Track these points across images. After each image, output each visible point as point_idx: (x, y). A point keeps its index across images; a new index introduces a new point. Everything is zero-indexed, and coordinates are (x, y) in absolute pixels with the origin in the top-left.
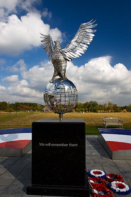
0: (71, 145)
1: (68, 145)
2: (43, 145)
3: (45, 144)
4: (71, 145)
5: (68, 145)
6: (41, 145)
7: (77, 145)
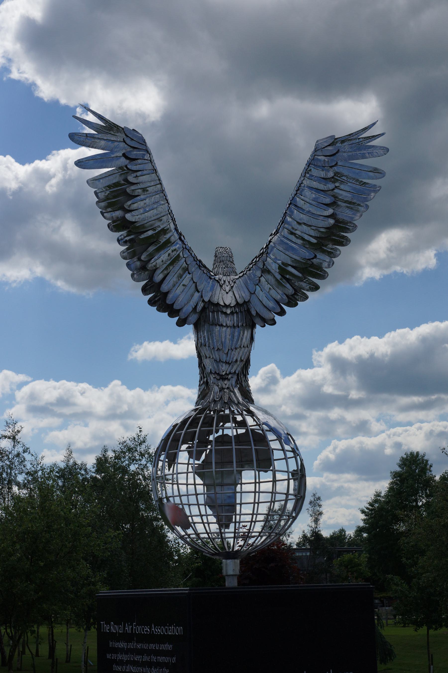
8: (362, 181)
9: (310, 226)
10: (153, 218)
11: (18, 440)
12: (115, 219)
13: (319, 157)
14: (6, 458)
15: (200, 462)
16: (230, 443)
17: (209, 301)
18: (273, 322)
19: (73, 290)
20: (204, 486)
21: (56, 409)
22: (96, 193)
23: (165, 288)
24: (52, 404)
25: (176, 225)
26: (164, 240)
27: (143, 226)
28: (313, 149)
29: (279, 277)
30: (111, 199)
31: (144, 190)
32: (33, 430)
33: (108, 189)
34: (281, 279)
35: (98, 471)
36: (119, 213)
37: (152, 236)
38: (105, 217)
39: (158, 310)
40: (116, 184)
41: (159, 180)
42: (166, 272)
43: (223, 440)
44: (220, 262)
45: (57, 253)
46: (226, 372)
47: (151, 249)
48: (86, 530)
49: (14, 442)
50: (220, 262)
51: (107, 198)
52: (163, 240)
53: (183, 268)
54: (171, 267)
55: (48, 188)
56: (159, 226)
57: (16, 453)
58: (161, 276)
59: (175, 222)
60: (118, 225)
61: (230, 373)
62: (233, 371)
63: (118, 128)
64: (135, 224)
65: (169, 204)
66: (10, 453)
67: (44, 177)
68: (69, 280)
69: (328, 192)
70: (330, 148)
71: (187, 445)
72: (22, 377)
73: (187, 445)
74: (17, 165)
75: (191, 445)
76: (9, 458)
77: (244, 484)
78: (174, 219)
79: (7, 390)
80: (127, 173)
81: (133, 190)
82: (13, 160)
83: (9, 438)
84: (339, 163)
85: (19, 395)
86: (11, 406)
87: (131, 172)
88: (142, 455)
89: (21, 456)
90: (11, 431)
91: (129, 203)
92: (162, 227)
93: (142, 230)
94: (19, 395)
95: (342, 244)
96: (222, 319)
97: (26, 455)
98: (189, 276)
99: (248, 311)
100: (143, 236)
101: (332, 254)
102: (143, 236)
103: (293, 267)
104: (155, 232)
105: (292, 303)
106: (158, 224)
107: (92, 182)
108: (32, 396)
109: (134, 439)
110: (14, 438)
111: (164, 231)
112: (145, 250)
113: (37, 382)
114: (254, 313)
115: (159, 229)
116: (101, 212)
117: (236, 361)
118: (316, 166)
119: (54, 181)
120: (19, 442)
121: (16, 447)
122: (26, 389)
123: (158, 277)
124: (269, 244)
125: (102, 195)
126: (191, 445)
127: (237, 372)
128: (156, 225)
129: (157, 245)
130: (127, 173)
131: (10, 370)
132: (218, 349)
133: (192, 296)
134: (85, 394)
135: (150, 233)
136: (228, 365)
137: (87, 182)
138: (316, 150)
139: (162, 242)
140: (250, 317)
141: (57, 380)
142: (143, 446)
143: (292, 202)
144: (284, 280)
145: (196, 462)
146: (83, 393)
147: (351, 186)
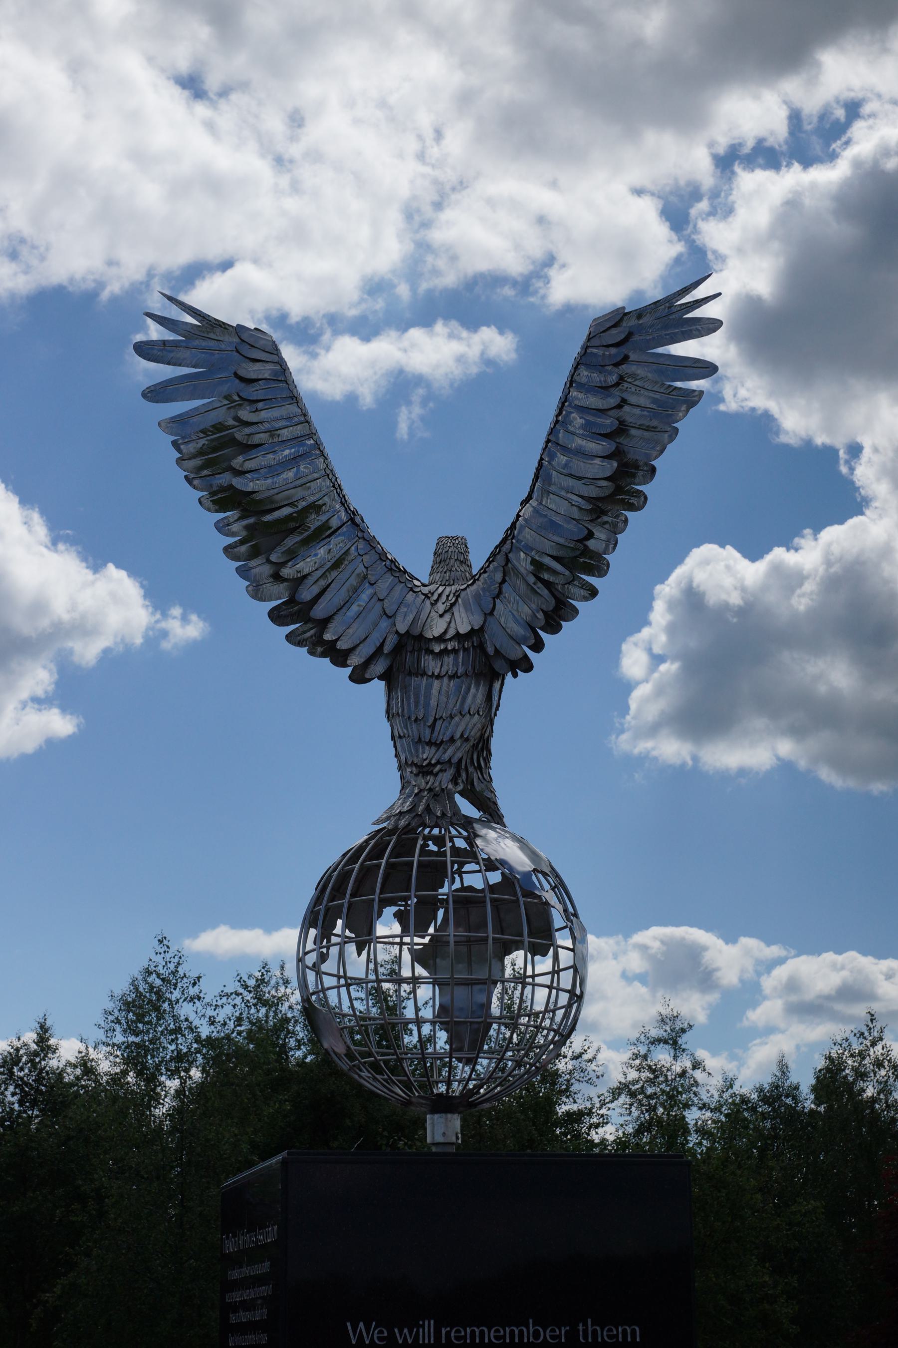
0: (587, 1330)
1: (572, 1335)
2: (375, 1334)
3: (392, 1334)
4: (594, 1333)
5: (572, 1335)
6: (405, 1339)
7: (633, 1332)
8: (670, 386)
9: (580, 478)
10: (292, 485)
11: (683, 1047)
12: (215, 488)
13: (595, 351)
14: (661, 1079)
15: (427, 940)
16: (481, 902)
17: (408, 632)
18: (528, 667)
19: (851, 783)
20: (434, 987)
21: (839, 1007)
22: (175, 444)
23: (319, 611)
24: (828, 998)
25: (344, 497)
26: (318, 524)
27: (270, 499)
28: (584, 337)
29: (531, 579)
30: (209, 454)
31: (272, 432)
32: (798, 1047)
33: (202, 435)
34: (534, 584)
35: (818, 1101)
36: (225, 479)
37: (289, 518)
38: (194, 487)
39: (311, 653)
40: (219, 427)
41: (305, 415)
42: (323, 583)
43: (467, 900)
44: (440, 562)
45: (812, 715)
46: (431, 760)
47: (291, 541)
48: (752, 1198)
49: (675, 1050)
50: (440, 562)
51: (200, 453)
52: (314, 522)
53: (359, 575)
54: (334, 574)
55: (794, 601)
56: (303, 499)
57: (679, 1070)
58: (316, 590)
59: (341, 490)
60: (224, 500)
61: (438, 762)
62: (446, 757)
63: (225, 328)
64: (254, 495)
65: (326, 458)
66: (668, 1070)
67: (791, 580)
68: (839, 763)
69: (611, 413)
70: (614, 331)
71: (397, 908)
72: (775, 951)
73: (397, 908)
74: (745, 563)
75: (403, 908)
76: (666, 1080)
77: (490, 975)
78: (339, 486)
79: (750, 975)
80: (240, 405)
81: (249, 435)
82: (738, 555)
83: (666, 1042)
84: (633, 357)
85: (769, 983)
86: (754, 1005)
87: (246, 403)
88: (879, 1064)
89: (687, 1075)
90: (668, 1029)
91: (240, 459)
92: (311, 499)
93: (268, 507)
94: (769, 983)
95: (632, 508)
96: (432, 665)
97: (698, 1075)
98: (369, 591)
99: (481, 647)
100: (267, 518)
101: (617, 528)
102: (267, 518)
103: (554, 558)
104: (296, 509)
105: (553, 627)
106: (299, 493)
107: (177, 424)
108: (792, 985)
109: (862, 1034)
110: (675, 1043)
111: (315, 508)
112: (279, 543)
113: (804, 958)
114: (490, 650)
115: (304, 504)
116: (186, 477)
117: (452, 740)
118: (588, 366)
119: (809, 587)
120: (684, 1050)
121: (679, 1059)
122: (781, 973)
123: (306, 594)
124: (517, 519)
125: (191, 448)
126: (403, 908)
127: (455, 760)
128: (299, 496)
129: (302, 533)
130: (240, 405)
131: (753, 937)
132: (416, 720)
133: (376, 625)
134: (892, 980)
135: (286, 511)
136: (433, 749)
137: (159, 424)
138: (589, 338)
139: (313, 527)
140: (490, 663)
141: (839, 952)
142: (879, 1048)
143: (552, 438)
144: (540, 585)
145: (417, 940)
146: (889, 976)
147: (649, 397)
